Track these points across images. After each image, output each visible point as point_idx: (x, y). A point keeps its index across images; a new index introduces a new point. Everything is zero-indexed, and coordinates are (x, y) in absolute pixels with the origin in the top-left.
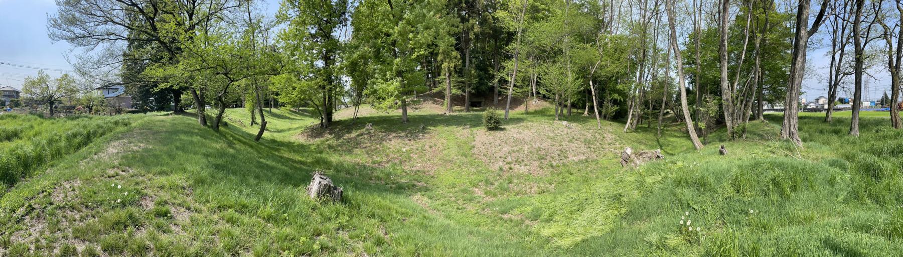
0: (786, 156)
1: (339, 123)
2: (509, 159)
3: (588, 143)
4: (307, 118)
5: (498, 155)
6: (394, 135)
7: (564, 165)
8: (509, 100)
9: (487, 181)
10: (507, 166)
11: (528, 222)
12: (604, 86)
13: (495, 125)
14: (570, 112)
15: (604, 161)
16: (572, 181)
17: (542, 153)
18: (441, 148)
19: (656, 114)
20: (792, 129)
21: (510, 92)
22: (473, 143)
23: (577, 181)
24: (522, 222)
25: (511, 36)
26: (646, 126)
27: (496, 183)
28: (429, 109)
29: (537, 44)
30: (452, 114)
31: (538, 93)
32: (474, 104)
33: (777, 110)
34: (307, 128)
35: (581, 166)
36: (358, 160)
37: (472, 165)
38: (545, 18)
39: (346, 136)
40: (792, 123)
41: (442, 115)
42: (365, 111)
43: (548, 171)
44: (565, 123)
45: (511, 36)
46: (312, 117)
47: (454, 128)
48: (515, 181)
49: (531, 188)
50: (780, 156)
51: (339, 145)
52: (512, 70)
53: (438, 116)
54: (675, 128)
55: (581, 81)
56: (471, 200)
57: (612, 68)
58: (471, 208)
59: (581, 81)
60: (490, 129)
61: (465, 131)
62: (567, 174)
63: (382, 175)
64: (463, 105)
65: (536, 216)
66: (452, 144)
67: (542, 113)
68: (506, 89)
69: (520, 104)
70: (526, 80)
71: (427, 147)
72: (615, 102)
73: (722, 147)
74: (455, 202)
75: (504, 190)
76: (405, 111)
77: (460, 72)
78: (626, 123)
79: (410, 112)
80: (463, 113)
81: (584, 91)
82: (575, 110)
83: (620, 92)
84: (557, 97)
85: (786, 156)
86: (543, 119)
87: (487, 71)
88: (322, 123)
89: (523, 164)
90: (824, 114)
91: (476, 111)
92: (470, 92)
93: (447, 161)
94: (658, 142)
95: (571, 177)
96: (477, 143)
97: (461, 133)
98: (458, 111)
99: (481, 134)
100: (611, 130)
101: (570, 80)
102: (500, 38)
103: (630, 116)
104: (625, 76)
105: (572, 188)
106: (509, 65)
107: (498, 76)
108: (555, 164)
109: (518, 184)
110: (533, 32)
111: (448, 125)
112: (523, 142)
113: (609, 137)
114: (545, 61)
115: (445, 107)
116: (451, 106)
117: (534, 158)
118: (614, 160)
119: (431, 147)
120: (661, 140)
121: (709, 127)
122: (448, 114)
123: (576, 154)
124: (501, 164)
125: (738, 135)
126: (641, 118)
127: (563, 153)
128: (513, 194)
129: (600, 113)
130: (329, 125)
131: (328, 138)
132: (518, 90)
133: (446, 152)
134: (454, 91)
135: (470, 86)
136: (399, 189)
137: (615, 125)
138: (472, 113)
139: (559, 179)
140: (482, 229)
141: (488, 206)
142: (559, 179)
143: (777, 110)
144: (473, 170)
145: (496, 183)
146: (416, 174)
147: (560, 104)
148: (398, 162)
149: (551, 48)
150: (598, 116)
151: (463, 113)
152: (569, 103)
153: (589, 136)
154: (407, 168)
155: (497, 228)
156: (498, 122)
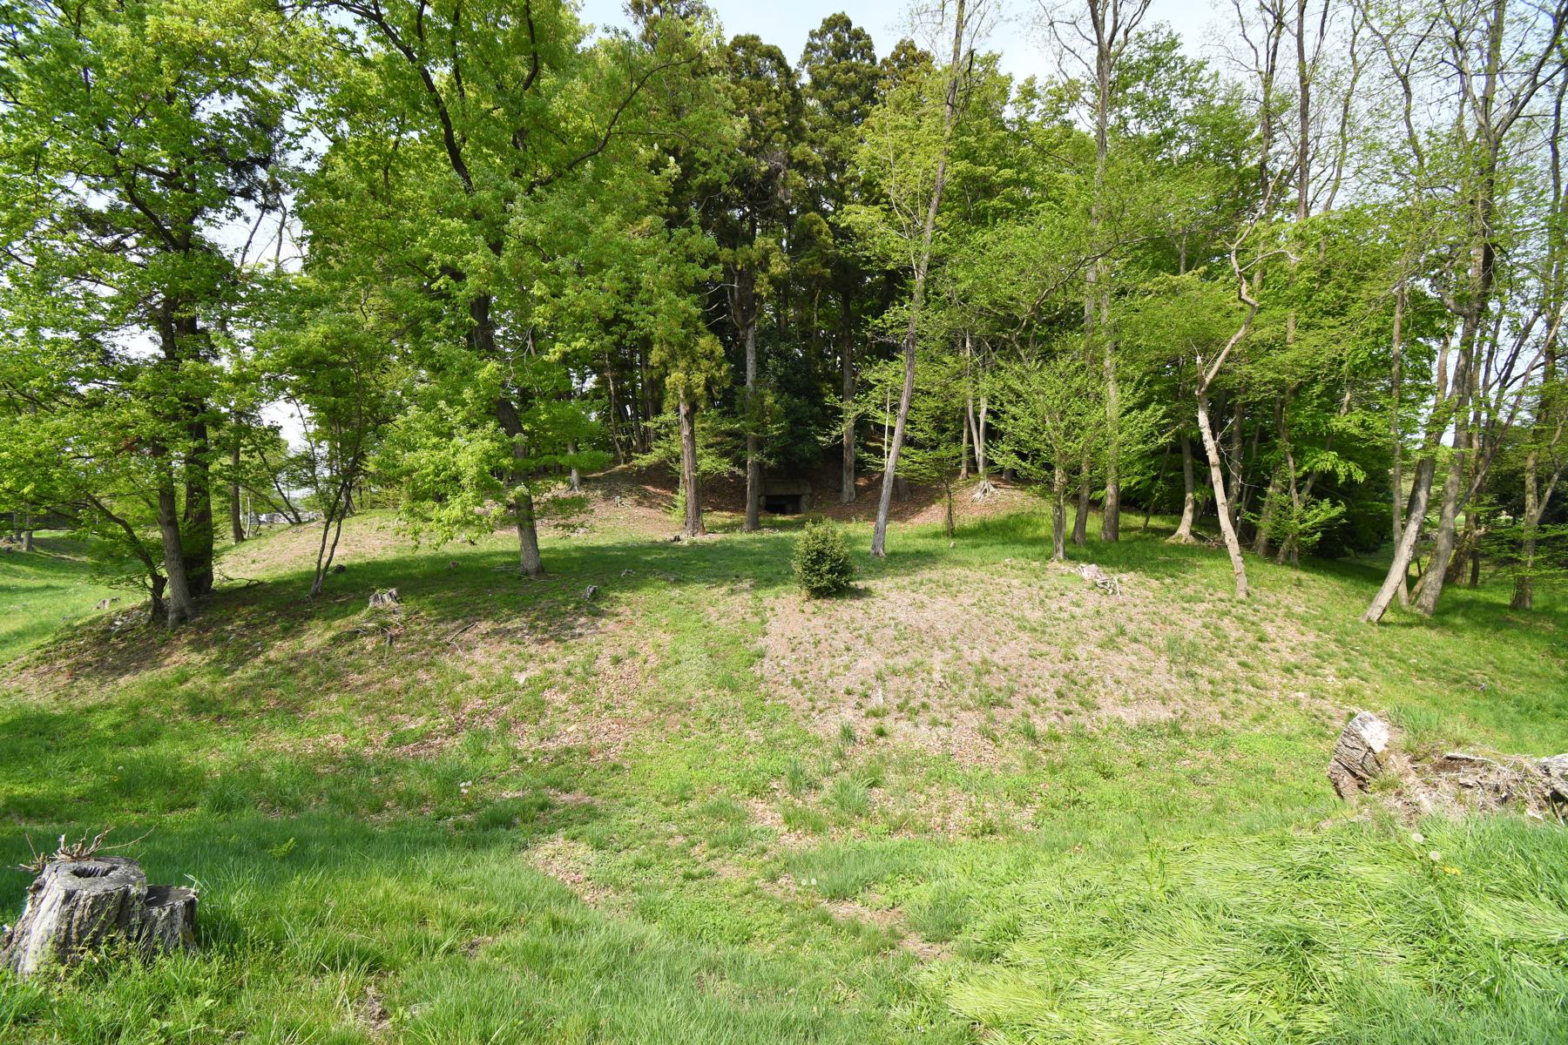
1: (251, 593)
2: (877, 700)
3: (1184, 656)
4: (81, 582)
6: (485, 626)
7: (1079, 736)
8: (886, 490)
9: (796, 775)
10: (871, 724)
11: (914, 944)
12: (1260, 427)
13: (834, 579)
14: (1114, 528)
15: (1255, 742)
16: (1107, 804)
17: (997, 681)
18: (654, 661)
21: (889, 463)
22: (761, 643)
23: (1124, 807)
24: (896, 937)
25: (895, 284)
26: (1505, 599)
27: (827, 784)
28: (619, 523)
29: (982, 300)
30: (701, 538)
31: (990, 463)
32: (775, 505)
34: (74, 632)
35: (1148, 748)
36: (335, 740)
37: (751, 718)
38: (1021, 209)
39: (280, 650)
41: (665, 546)
42: (371, 537)
43: (1014, 753)
44: (1089, 571)
45: (895, 284)
46: (100, 571)
47: (697, 592)
48: (892, 777)
49: (947, 810)
51: (242, 692)
52: (895, 393)
53: (654, 546)
55: (1155, 412)
56: (737, 843)
57: (1305, 348)
58: (733, 872)
59: (1155, 412)
60: (819, 593)
61: (736, 600)
62: (1088, 774)
63: (425, 786)
64: (738, 507)
65: (944, 925)
66: (691, 648)
67: (1003, 532)
68: (879, 452)
69: (930, 501)
70: (950, 423)
71: (604, 663)
72: (1324, 487)
74: (683, 852)
75: (852, 810)
76: (530, 535)
77: (726, 399)
78: (1380, 577)
79: (548, 537)
80: (739, 537)
81: (1175, 448)
82: (1138, 520)
83: (1344, 446)
84: (1059, 476)
87: (815, 397)
88: (158, 607)
89: (924, 717)
91: (783, 526)
92: (760, 466)
93: (669, 708)
95: (1107, 788)
96: (774, 643)
97: (723, 606)
98: (724, 529)
99: (789, 613)
100: (1299, 604)
101: (1112, 408)
102: (856, 294)
103: (1404, 553)
104: (1385, 375)
105: (1097, 837)
106: (883, 373)
107: (851, 410)
108: (1041, 727)
109: (901, 792)
110: (969, 265)
111: (679, 582)
112: (926, 637)
113: (1288, 639)
114: (1013, 356)
115: (676, 517)
116: (699, 512)
117: (965, 698)
118: (1311, 746)
119: (617, 661)
122: (686, 539)
124: (848, 715)
126: (1467, 559)
127: (1076, 689)
128: (882, 827)
129: (1247, 534)
130: (197, 602)
131: (186, 664)
132: (919, 456)
133: (669, 675)
134: (707, 463)
135: (759, 445)
136: (496, 827)
137: (1321, 589)
138: (767, 534)
139: (1054, 787)
140: (756, 952)
141: (790, 865)
142: (1054, 787)
144: (753, 735)
145: (827, 784)
146: (558, 760)
147: (1075, 499)
148: (491, 725)
149: (1037, 309)
150: (1233, 547)
151: (739, 537)
152: (1109, 495)
153: (1191, 626)
154: (526, 741)
155: (806, 953)
156: (843, 569)
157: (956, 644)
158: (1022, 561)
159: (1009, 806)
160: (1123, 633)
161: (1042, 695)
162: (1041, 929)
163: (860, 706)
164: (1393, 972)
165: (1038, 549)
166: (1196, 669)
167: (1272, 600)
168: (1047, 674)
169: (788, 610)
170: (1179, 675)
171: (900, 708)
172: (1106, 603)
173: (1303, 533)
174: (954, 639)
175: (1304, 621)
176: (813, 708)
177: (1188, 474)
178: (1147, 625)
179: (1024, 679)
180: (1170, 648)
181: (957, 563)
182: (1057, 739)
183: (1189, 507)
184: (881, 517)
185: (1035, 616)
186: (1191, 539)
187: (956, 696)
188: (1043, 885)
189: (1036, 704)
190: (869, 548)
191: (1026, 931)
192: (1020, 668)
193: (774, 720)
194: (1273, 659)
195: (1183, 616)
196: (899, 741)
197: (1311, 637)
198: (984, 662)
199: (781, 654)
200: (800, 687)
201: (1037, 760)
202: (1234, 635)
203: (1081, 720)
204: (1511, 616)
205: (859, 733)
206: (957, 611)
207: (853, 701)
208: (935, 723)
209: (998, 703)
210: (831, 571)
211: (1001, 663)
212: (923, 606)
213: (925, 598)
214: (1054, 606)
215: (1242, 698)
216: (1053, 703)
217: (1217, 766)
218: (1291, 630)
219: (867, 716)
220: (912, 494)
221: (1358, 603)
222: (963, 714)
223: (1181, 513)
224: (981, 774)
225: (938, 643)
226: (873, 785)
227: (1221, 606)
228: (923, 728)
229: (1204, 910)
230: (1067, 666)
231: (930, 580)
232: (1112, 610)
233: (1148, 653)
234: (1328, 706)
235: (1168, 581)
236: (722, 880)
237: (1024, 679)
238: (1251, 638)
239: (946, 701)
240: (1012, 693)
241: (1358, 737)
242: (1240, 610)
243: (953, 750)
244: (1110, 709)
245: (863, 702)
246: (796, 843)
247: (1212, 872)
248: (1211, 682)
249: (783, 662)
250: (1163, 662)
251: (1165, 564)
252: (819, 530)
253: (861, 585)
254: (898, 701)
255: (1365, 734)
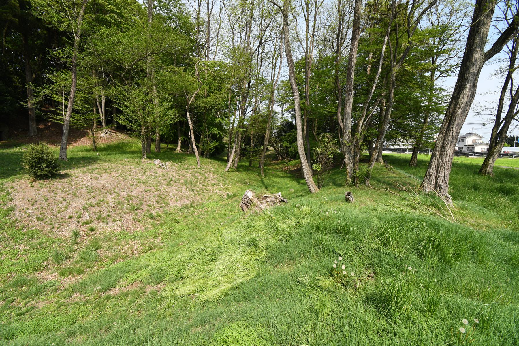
0: (434, 214)
2: (86, 217)
3: (190, 185)
5: (66, 215)
7: (166, 213)
8: (65, 131)
10: (86, 228)
13: (47, 170)
14: (159, 148)
16: (181, 230)
17: (136, 201)
19: (261, 152)
20: (440, 182)
22: (10, 205)
24: (143, 290)
33: (395, 150)
35: (187, 212)
40: (441, 174)
43: (147, 224)
44: (157, 162)
49: (132, 248)
50: (423, 212)
54: (276, 167)
62: (172, 224)
67: (119, 149)
73: (349, 194)
85: (434, 214)
86: (125, 158)
89: (110, 220)
90: (479, 161)
94: (263, 182)
100: (210, 169)
104: (227, 108)
106: (61, 78)
108: (154, 214)
112: (103, 190)
114: (122, 82)
117: (125, 209)
120: (266, 181)
121: (324, 169)
123: (178, 199)
124: (73, 226)
125: (359, 180)
127: (162, 199)
128: (110, 262)
139: (165, 230)
141: (74, 289)
142: (165, 230)
143: (395, 150)
144: (21, 247)
152: (157, 136)
157: (117, 191)
158: (132, 160)
159: (152, 240)
160: (172, 180)
161: (152, 203)
162: (190, 265)
163: (78, 222)
164: (272, 240)
165: (135, 155)
166: (193, 188)
167: (206, 168)
168: (152, 196)
169: (23, 187)
170: (189, 190)
171: (98, 219)
172: (165, 172)
173: (210, 149)
174: (115, 189)
175: (214, 172)
176: (54, 228)
177: (179, 131)
178: (178, 177)
179: (145, 199)
180: (185, 183)
181: (104, 161)
182: (160, 216)
183: (180, 142)
184: (64, 141)
185: (143, 178)
186: (181, 151)
187: (121, 209)
188: (182, 255)
189: (150, 206)
190: (58, 156)
191: (187, 267)
192: (142, 196)
193: (32, 238)
194: (209, 183)
195: (186, 174)
196: (101, 231)
197: (216, 176)
198: (129, 196)
199: (26, 207)
200: (42, 220)
201: (157, 224)
202: (199, 178)
203: (166, 208)
204: (250, 168)
205: (81, 232)
206: (113, 179)
207: (74, 221)
208: (115, 221)
209: (138, 209)
210: (47, 167)
211: (135, 195)
212: (97, 179)
213: (97, 175)
214: (149, 174)
215: (205, 194)
216: (156, 205)
217: (203, 212)
218: (211, 175)
219: (83, 225)
220: (76, 133)
221: (223, 167)
222: (125, 215)
223: (178, 143)
224: (139, 233)
225: (108, 192)
226: (98, 249)
227: (195, 170)
228: (110, 224)
229: (232, 242)
230: (158, 193)
231: (97, 168)
232: (167, 174)
233: (180, 186)
234: (222, 192)
235: (180, 164)
236: (41, 308)
237: (145, 199)
238: (203, 178)
239: (117, 212)
240: (142, 204)
241: (246, 196)
242: (199, 171)
243: (125, 228)
244: (174, 204)
245: (80, 220)
246: (67, 282)
247: (228, 234)
248: (197, 191)
249: (28, 211)
250: (184, 187)
251: (176, 159)
252: (39, 147)
253: (62, 172)
254: (96, 216)
255: (248, 195)
